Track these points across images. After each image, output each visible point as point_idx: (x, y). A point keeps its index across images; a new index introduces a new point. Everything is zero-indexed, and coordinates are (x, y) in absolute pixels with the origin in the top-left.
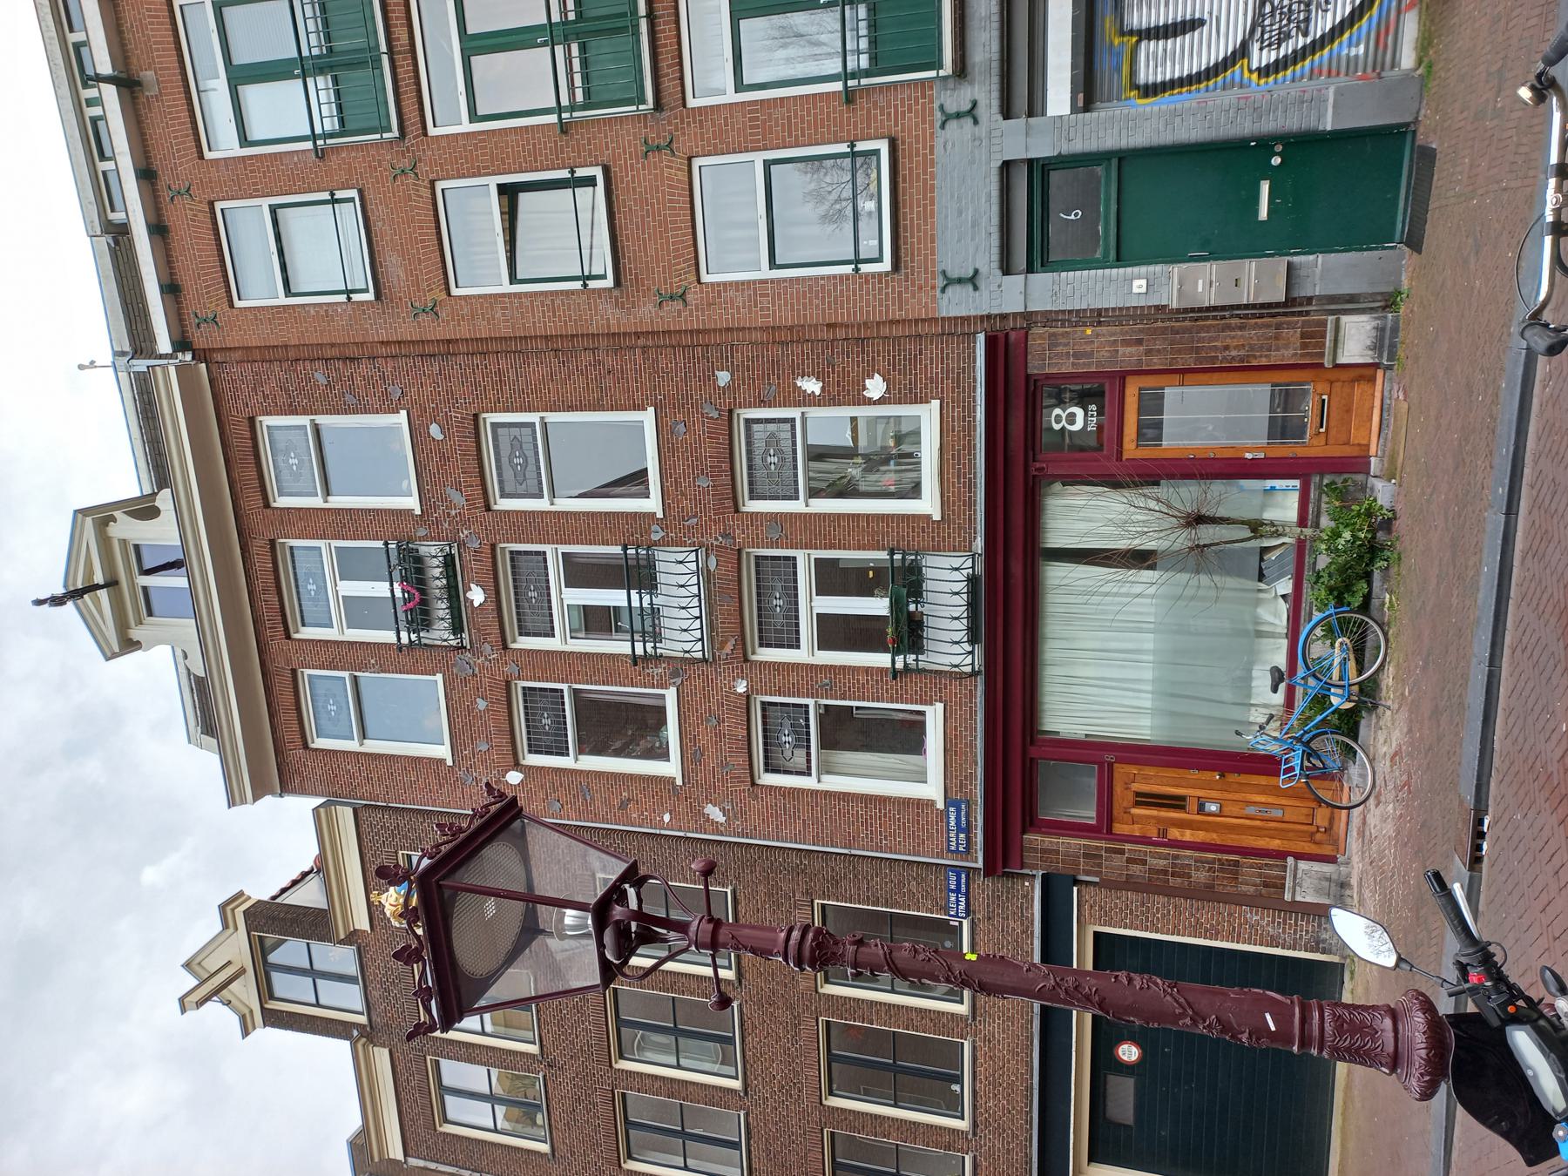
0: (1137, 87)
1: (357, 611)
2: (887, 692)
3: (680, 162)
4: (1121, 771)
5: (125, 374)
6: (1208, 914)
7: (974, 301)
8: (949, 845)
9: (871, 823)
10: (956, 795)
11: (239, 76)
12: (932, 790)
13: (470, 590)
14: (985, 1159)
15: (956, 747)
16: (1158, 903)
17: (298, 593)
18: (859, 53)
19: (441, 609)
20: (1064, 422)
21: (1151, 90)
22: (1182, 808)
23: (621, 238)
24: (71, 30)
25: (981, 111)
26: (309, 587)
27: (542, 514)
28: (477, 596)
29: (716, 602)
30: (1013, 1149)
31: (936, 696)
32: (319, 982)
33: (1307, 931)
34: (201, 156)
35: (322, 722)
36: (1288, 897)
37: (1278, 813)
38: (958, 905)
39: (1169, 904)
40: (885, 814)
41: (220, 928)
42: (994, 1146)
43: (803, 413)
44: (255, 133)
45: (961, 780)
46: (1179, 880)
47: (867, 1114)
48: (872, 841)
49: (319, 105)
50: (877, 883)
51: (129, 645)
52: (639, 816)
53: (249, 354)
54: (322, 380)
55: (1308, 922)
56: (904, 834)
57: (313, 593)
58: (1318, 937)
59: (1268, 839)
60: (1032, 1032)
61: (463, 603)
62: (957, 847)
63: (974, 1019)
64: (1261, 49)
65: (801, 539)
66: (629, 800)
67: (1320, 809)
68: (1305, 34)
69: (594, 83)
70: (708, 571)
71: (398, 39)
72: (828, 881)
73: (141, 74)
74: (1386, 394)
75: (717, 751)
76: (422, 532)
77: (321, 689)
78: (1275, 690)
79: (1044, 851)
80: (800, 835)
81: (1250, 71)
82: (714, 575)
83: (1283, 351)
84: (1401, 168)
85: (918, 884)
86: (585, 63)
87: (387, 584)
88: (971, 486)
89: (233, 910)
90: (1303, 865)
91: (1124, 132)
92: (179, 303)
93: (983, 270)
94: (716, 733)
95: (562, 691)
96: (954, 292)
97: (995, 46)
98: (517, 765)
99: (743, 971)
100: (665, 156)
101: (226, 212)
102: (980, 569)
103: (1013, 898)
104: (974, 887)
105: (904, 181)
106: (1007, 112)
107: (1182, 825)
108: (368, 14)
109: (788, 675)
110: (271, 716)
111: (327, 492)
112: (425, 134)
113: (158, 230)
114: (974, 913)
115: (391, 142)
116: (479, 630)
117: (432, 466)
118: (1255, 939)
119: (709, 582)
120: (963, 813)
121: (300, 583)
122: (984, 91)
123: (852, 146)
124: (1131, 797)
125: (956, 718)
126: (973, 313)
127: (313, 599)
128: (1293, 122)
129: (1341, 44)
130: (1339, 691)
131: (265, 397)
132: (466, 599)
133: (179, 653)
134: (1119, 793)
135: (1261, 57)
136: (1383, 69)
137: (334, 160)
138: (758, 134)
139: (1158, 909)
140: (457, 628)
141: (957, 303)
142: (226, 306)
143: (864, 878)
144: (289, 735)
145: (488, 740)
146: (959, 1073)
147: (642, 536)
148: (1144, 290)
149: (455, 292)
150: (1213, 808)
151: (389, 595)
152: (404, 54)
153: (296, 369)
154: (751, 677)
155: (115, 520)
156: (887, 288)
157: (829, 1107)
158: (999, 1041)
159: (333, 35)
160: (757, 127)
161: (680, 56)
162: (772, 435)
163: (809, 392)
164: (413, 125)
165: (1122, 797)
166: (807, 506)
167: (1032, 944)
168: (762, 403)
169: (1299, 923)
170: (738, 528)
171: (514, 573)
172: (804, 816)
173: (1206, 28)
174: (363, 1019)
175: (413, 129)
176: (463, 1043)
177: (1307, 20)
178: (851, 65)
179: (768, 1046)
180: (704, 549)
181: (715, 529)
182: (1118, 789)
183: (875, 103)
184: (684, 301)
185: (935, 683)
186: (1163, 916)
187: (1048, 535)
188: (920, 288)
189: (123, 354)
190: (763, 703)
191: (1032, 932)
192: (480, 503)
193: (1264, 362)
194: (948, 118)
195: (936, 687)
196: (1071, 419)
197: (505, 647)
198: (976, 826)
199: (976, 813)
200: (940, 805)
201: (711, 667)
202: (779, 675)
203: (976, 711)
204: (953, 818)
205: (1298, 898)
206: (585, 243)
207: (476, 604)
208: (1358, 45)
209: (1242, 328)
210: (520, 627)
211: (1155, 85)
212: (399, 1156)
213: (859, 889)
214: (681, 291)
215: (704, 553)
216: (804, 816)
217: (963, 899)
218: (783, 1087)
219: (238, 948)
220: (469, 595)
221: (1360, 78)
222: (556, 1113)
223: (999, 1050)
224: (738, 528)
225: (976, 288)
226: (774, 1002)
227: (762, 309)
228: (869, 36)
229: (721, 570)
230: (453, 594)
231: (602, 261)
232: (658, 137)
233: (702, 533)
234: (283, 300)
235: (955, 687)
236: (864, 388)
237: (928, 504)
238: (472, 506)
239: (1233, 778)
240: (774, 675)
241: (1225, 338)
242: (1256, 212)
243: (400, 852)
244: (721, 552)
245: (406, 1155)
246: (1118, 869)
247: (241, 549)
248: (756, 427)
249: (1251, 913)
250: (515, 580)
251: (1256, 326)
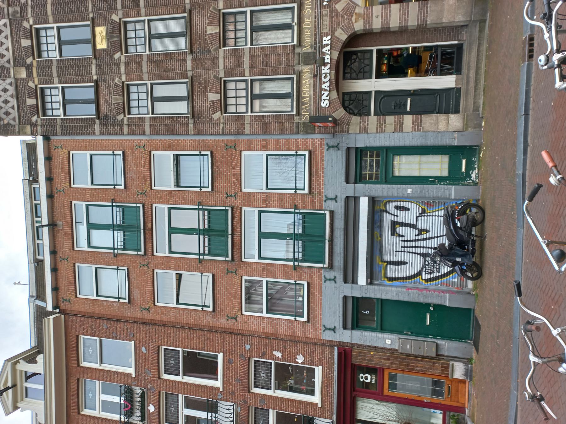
0: (387, 278)
1: (106, 406)
3: (238, 277)
5: (32, 304)
7: (334, 336)
11: (91, 227)
17: (85, 396)
18: (299, 252)
19: (137, 413)
20: (364, 379)
21: (391, 279)
23: (217, 297)
24: (35, 200)
25: (337, 280)
28: (152, 408)
34: (73, 249)
44: (94, 244)
49: (117, 220)
51: (15, 408)
53: (80, 315)
54: (105, 327)
64: (425, 274)
68: (439, 272)
69: (212, 246)
70: (237, 412)
71: (147, 226)
73: (57, 222)
74: (470, 389)
81: (422, 279)
83: (435, 371)
84: (470, 319)
86: (209, 218)
88: (332, 397)
91: (383, 294)
92: (50, 164)
93: (337, 327)
95: (179, 351)
96: (329, 202)
97: (342, 262)
100: (234, 275)
101: (74, 155)
105: (312, 296)
106: (346, 281)
108: (138, 214)
111: (101, 362)
112: (153, 255)
113: (54, 270)
115: (140, 255)
116: (151, 421)
117: (141, 361)
119: (237, 416)
122: (338, 274)
123: (296, 152)
126: (333, 340)
127: (91, 399)
128: (437, 301)
129: (450, 277)
131: (84, 329)
132: (148, 409)
133: (34, 415)
135: (425, 276)
136: (463, 287)
137: (120, 258)
138: (265, 273)
141: (328, 336)
142: (74, 297)
144: (73, 406)
148: (390, 343)
149: (153, 188)
152: (149, 231)
153: (96, 322)
155: (19, 363)
156: (305, 327)
159: (125, 222)
160: (265, 271)
161: (241, 247)
163: (277, 356)
164: (149, 252)
171: (166, 400)
173: (408, 265)
175: (149, 253)
177: (439, 269)
178: (296, 256)
183: (303, 271)
184: (236, 198)
187: (358, 415)
188: (316, 329)
189: (33, 296)
190: (255, 360)
193: (429, 373)
194: (326, 280)
196: (366, 378)
206: (204, 293)
207: (151, 412)
208: (455, 279)
209: (422, 361)
210: (166, 420)
211: (392, 278)
214: (235, 316)
220: (149, 408)
221: (456, 288)
225: (335, 332)
227: (263, 326)
228: (302, 248)
231: (209, 301)
232: (232, 269)
234: (95, 297)
236: (296, 358)
237: (316, 399)
238: (154, 377)
241: (417, 363)
242: (426, 323)
247: (66, 380)
250: (166, 403)
251: (426, 361)
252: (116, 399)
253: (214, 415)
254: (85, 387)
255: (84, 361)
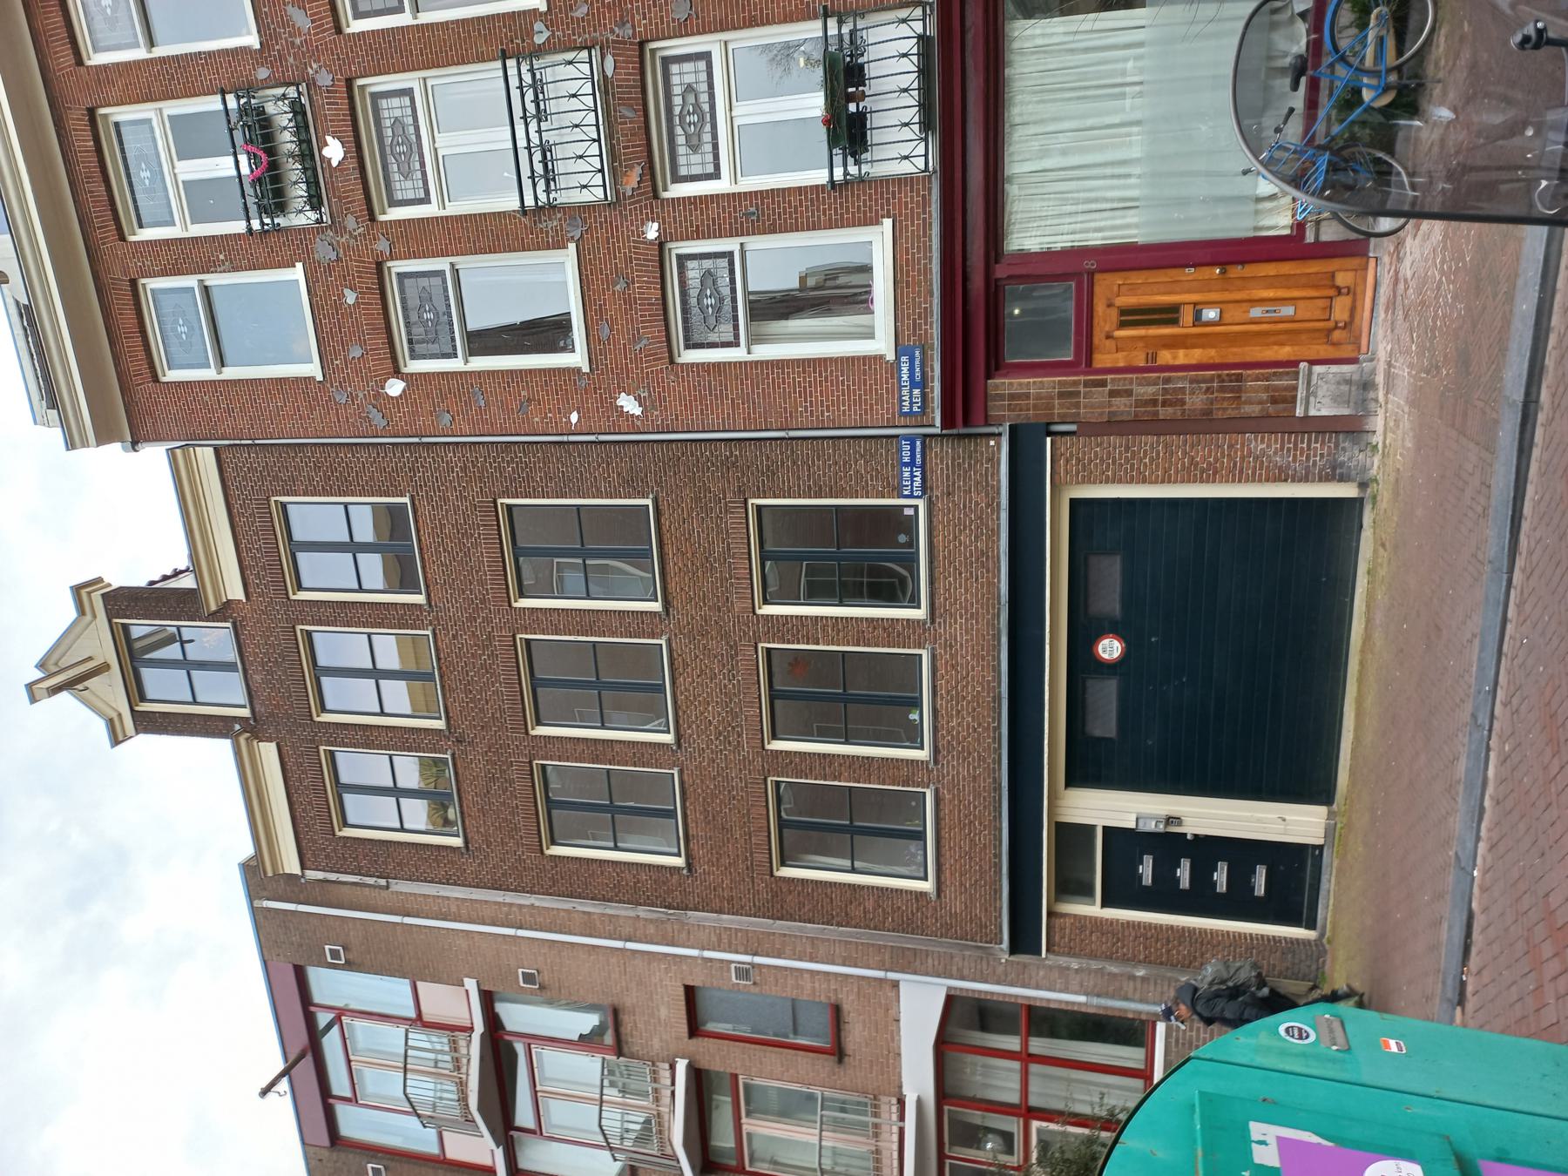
1: (200, 196)
2: (825, 214)
4: (1106, 285)
6: (1204, 450)
8: (901, 406)
9: (811, 392)
10: (909, 340)
12: (882, 344)
13: (326, 145)
14: (949, 791)
15: (908, 276)
16: (1146, 444)
22: (1174, 322)
26: (143, 174)
27: (402, 30)
28: (334, 151)
29: (616, 119)
30: (980, 775)
31: (882, 209)
32: (194, 673)
33: (1322, 455)
35: (173, 349)
36: (1299, 412)
37: (1288, 311)
38: (912, 481)
39: (1158, 443)
40: (826, 378)
41: (72, 614)
42: (958, 773)
43: (742, 244)
45: (914, 320)
46: (1170, 410)
47: (814, 754)
48: (812, 416)
50: (819, 467)
52: (542, 419)
55: (1323, 443)
56: (849, 400)
57: (147, 182)
58: (1335, 460)
59: (1276, 347)
60: (999, 630)
61: (318, 163)
62: (911, 408)
63: (933, 621)
65: (715, 16)
66: (529, 400)
67: (1339, 299)
70: (605, 77)
72: (763, 473)
75: (628, 324)
76: (263, 73)
77: (167, 304)
78: (1295, 87)
79: (1012, 397)
80: (729, 419)
82: (612, 83)
85: (866, 462)
87: (231, 159)
89: (89, 593)
90: (1318, 369)
94: (625, 300)
98: (397, 373)
99: (670, 598)
102: (932, 31)
103: (976, 463)
104: (931, 455)
107: (1174, 343)
109: (707, 208)
110: (112, 343)
111: (222, 363)
114: (932, 489)
116: (339, 197)
118: (1261, 475)
119: (607, 93)
120: (917, 362)
121: (132, 171)
124: (1114, 313)
125: (907, 237)
130: (1374, 82)
134: (1100, 314)
139: (1145, 451)
140: (315, 201)
143: (804, 463)
144: (136, 365)
145: (363, 344)
146: (918, 695)
147: (523, 41)
150: (1211, 314)
151: (234, 173)
154: (664, 218)
157: (772, 751)
158: (962, 645)
162: (708, 273)
165: (1105, 318)
166: (749, 353)
167: (998, 519)
168: (698, 235)
169: (1313, 445)
170: (638, 13)
172: (732, 394)
174: (246, 713)
176: (360, 725)
179: (702, 685)
180: (598, 47)
181: (610, 18)
182: (1100, 308)
185: (882, 193)
186: (1152, 460)
191: (999, 504)
192: (328, 23)
195: (882, 198)
197: (372, 218)
198: (933, 377)
199: (932, 360)
200: (891, 357)
201: (615, 209)
202: (696, 210)
203: (930, 224)
204: (905, 370)
205: (1312, 413)
207: (335, 163)
212: (296, 870)
213: (799, 478)
215: (599, 53)
216: (732, 394)
217: (918, 474)
218: (720, 734)
219: (100, 644)
220: (326, 152)
222: (469, 798)
223: (962, 655)
224: (638, 13)
226: (707, 632)
229: (620, 74)
230: (308, 154)
233: (594, 26)
235: (906, 196)
239: (1236, 271)
240: (690, 210)
243: (273, 499)
244: (619, 49)
245: (303, 867)
246: (1099, 407)
247: (55, 125)
248: (691, 264)
249: (1256, 440)
252: (223, 166)
253: (633, 1135)
254: (123, 151)
255: (96, 50)
